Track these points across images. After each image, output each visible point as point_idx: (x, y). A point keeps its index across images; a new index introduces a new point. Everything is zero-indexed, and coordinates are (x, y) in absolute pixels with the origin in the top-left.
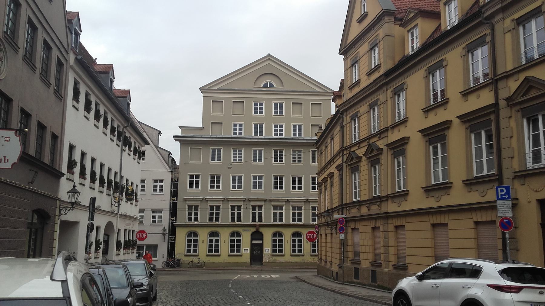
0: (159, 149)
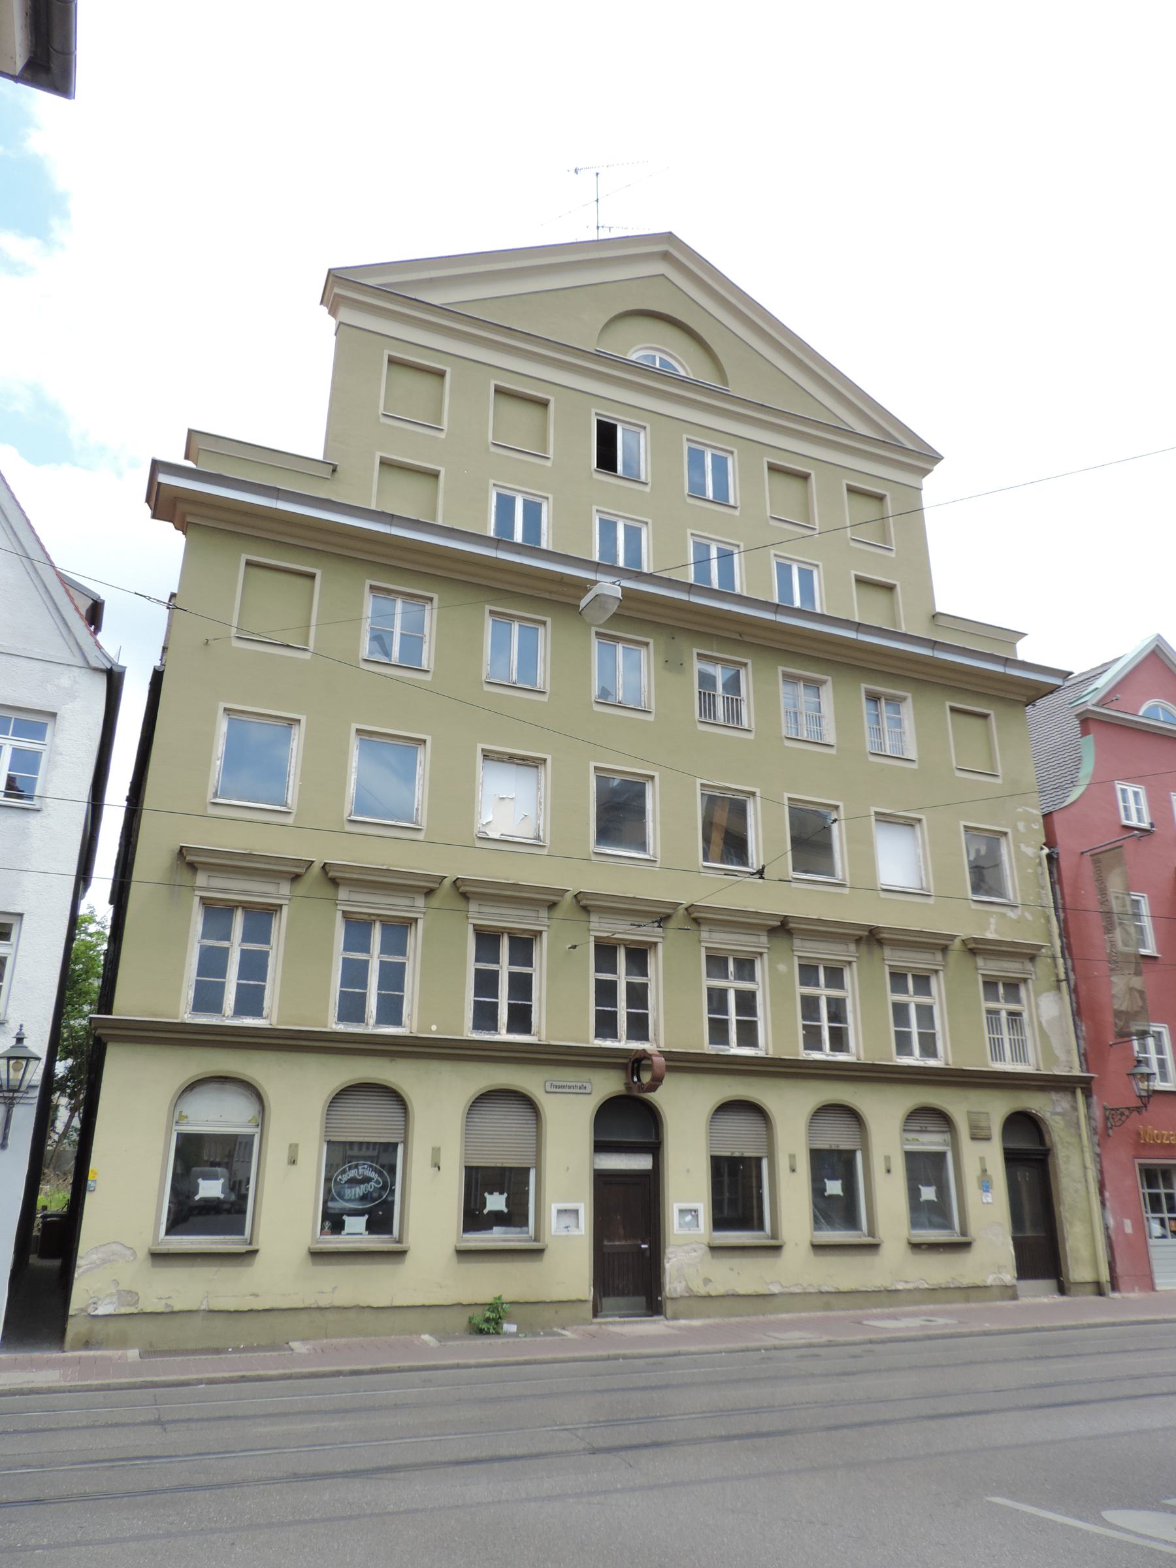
0: (72, 591)
